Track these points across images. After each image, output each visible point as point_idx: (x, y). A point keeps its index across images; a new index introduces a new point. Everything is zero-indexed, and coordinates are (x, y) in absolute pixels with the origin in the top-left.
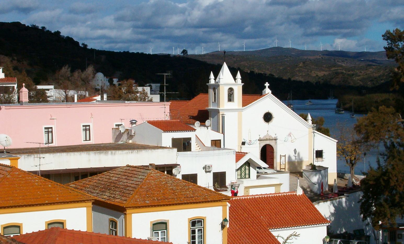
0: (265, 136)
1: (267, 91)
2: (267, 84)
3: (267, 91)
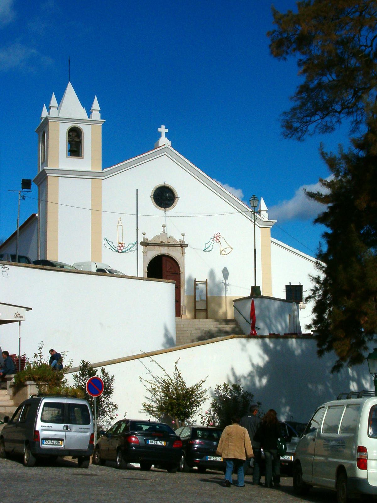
0: (158, 237)
1: (164, 141)
2: (163, 130)
3: (164, 141)
